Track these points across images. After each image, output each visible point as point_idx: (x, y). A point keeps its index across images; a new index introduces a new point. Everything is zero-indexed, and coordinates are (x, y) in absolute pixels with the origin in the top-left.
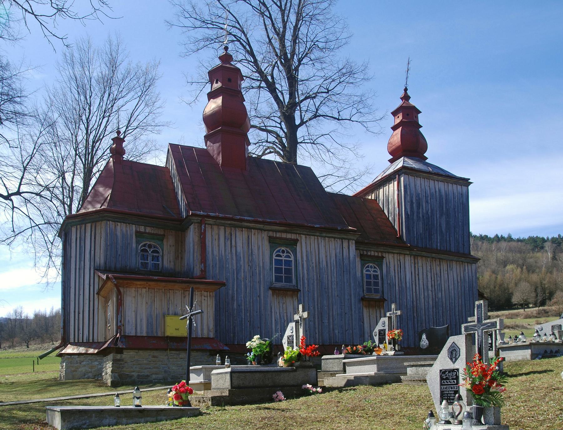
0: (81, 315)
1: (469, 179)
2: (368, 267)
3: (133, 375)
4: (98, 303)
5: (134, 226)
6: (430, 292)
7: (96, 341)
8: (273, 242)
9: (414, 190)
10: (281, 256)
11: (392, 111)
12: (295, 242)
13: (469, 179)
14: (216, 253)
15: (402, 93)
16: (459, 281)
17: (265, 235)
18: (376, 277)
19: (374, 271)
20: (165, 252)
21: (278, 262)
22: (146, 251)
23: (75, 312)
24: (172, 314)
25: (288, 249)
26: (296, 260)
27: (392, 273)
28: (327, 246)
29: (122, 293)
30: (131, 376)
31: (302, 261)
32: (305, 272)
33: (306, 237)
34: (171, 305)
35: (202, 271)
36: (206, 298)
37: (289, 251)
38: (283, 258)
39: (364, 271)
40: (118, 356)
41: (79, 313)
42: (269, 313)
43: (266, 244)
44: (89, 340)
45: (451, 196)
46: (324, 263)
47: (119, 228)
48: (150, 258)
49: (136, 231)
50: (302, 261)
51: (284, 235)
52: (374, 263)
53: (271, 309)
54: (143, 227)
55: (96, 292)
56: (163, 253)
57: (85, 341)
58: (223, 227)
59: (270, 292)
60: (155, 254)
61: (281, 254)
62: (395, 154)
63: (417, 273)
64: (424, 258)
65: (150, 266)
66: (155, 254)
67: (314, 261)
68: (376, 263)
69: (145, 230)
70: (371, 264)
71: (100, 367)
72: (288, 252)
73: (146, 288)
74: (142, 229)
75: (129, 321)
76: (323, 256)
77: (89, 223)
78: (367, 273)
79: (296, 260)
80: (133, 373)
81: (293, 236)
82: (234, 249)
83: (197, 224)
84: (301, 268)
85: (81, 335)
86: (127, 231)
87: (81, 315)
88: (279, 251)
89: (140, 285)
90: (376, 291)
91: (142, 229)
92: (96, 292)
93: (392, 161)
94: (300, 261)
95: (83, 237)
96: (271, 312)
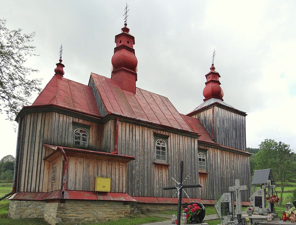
0: (30, 174)
1: (246, 113)
3: (72, 219)
4: (44, 167)
5: (72, 118)
6: (229, 170)
7: (40, 191)
8: (155, 135)
9: (56, 140)
11: (206, 75)
14: (124, 138)
15: (211, 66)
16: (242, 165)
17: (152, 131)
19: (203, 157)
20: (91, 137)
21: (158, 148)
22: (79, 134)
23: (26, 171)
24: (100, 176)
29: (67, 160)
30: (71, 220)
31: (171, 148)
36: (122, 167)
38: (161, 146)
40: (62, 205)
41: (29, 172)
42: (153, 177)
43: (152, 136)
44: (35, 190)
46: (182, 150)
47: (61, 119)
48: (81, 139)
49: (73, 121)
50: (171, 148)
51: (162, 132)
52: (203, 153)
54: (77, 119)
55: (43, 158)
57: (32, 191)
58: (129, 124)
59: (153, 166)
60: (84, 137)
61: (160, 143)
62: (207, 97)
64: (226, 152)
66: (84, 137)
68: (204, 152)
69: (79, 121)
70: (201, 153)
71: (43, 210)
73: (83, 158)
74: (77, 120)
75: (71, 180)
76: (181, 146)
77: (40, 112)
78: (203, 158)
80: (72, 217)
81: (167, 134)
83: (113, 120)
85: (29, 187)
87: (30, 174)
89: (80, 155)
91: (77, 120)
92: (43, 158)
93: (205, 100)
96: (154, 177)
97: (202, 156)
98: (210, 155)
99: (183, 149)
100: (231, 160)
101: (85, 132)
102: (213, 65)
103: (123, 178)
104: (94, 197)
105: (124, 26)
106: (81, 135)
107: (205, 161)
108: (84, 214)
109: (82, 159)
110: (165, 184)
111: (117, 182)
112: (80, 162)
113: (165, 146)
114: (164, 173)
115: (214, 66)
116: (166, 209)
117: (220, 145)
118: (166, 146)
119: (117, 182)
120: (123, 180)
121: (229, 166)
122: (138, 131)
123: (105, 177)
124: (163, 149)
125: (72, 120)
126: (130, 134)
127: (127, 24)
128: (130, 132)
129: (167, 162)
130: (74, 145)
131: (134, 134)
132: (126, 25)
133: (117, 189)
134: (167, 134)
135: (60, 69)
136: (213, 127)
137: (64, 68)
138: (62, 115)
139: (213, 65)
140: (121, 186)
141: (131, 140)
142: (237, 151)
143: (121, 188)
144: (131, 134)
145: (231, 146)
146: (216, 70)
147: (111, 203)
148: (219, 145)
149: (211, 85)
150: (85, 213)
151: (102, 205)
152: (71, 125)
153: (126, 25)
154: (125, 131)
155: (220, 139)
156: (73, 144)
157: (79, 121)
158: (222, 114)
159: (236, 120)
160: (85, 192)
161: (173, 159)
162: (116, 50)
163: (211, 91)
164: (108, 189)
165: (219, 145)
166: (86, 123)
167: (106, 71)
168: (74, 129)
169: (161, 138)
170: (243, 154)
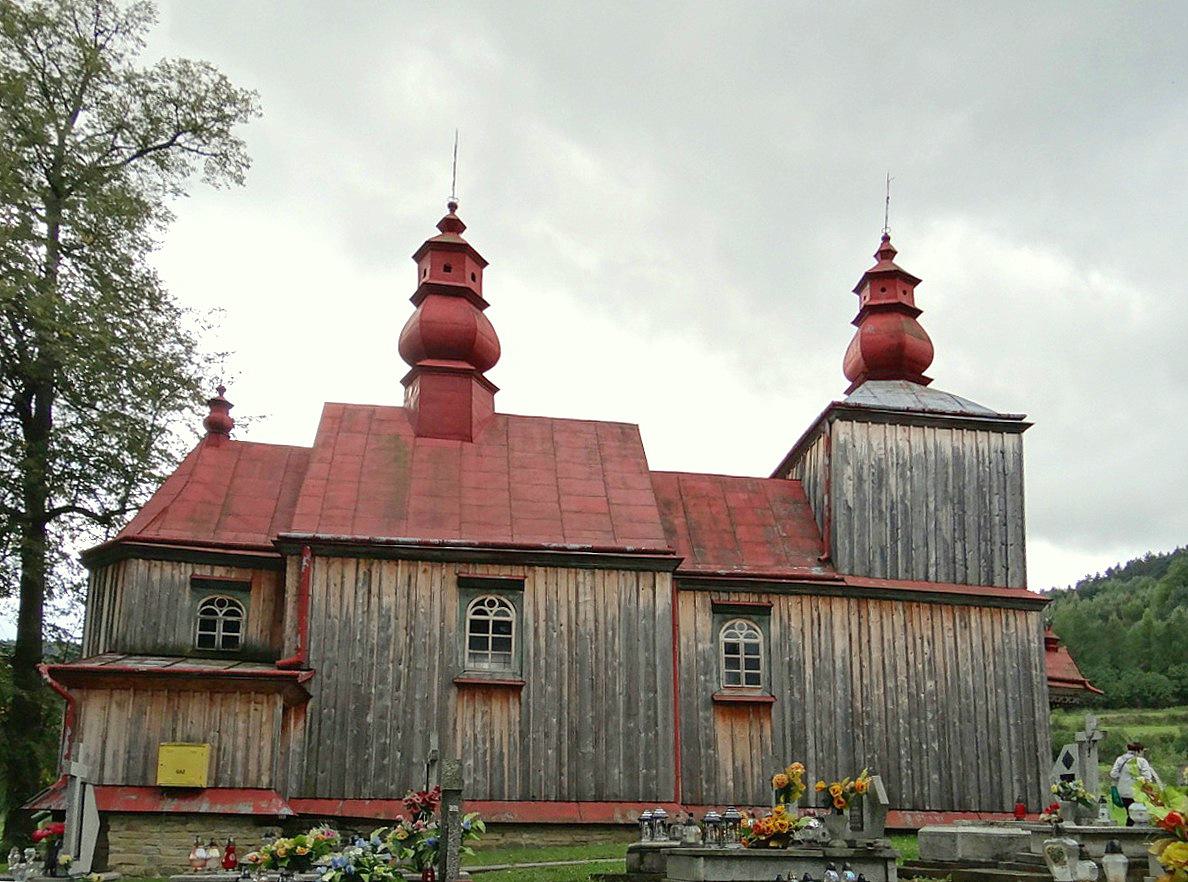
1: (1024, 417)
2: (732, 627)
8: (465, 584)
10: (485, 613)
12: (766, 610)
13: (1024, 417)
18: (752, 649)
25: (502, 598)
26: (521, 621)
27: (795, 637)
28: (599, 588)
31: (536, 621)
32: (542, 643)
33: (546, 571)
34: (180, 722)
35: (297, 649)
37: (506, 601)
39: (722, 636)
43: (452, 590)
45: (969, 459)
46: (591, 625)
47: (156, 576)
48: (220, 626)
50: (536, 621)
52: (750, 619)
53: (455, 724)
54: (208, 568)
56: (248, 617)
59: (454, 692)
60: (229, 619)
61: (487, 609)
63: (865, 640)
64: (886, 604)
65: (219, 641)
66: (229, 619)
67: (564, 620)
69: (212, 572)
72: (502, 604)
76: (587, 610)
79: (521, 621)
82: (374, 600)
84: (532, 634)
86: (173, 576)
88: (481, 603)
90: (753, 679)
94: (531, 622)
95: (101, 591)
96: (455, 729)
97: (745, 632)
98: (786, 629)
99: (596, 621)
100: (918, 636)
101: (232, 603)
102: (886, 238)
103: (260, 741)
104: (147, 804)
105: (447, 212)
106: (221, 615)
107: (762, 652)
108: (118, 852)
109: (125, 695)
110: (502, 753)
111: (240, 755)
112: (120, 705)
113: (508, 616)
114: (503, 717)
115: (891, 242)
116: (501, 842)
117: (843, 580)
118: (512, 617)
119: (240, 755)
120: (260, 749)
121: (901, 665)
122: (390, 579)
123: (199, 741)
124: (503, 627)
125: (190, 573)
126: (360, 594)
127: (458, 204)
128: (360, 584)
129: (519, 673)
130: (197, 647)
131: (375, 590)
132: (453, 207)
133: (239, 779)
134: (517, 572)
135: (217, 415)
136: (828, 506)
137: (230, 411)
138: (158, 563)
139: (886, 238)
140: (253, 767)
141: (364, 612)
142: (949, 596)
143: (253, 776)
144: (364, 593)
145: (921, 576)
146: (901, 262)
147: (210, 821)
148: (837, 580)
149: (877, 324)
150: (122, 850)
151: (176, 828)
152: (188, 588)
153: (453, 207)
154: (339, 586)
155: (859, 552)
156: (194, 646)
157: (212, 572)
158: (875, 444)
159: (958, 458)
160: (132, 789)
161: (542, 662)
162: (417, 299)
163: (860, 354)
164: (200, 780)
165: (837, 580)
166: (234, 575)
167: (384, 382)
168: (195, 599)
169: (494, 591)
170: (995, 604)
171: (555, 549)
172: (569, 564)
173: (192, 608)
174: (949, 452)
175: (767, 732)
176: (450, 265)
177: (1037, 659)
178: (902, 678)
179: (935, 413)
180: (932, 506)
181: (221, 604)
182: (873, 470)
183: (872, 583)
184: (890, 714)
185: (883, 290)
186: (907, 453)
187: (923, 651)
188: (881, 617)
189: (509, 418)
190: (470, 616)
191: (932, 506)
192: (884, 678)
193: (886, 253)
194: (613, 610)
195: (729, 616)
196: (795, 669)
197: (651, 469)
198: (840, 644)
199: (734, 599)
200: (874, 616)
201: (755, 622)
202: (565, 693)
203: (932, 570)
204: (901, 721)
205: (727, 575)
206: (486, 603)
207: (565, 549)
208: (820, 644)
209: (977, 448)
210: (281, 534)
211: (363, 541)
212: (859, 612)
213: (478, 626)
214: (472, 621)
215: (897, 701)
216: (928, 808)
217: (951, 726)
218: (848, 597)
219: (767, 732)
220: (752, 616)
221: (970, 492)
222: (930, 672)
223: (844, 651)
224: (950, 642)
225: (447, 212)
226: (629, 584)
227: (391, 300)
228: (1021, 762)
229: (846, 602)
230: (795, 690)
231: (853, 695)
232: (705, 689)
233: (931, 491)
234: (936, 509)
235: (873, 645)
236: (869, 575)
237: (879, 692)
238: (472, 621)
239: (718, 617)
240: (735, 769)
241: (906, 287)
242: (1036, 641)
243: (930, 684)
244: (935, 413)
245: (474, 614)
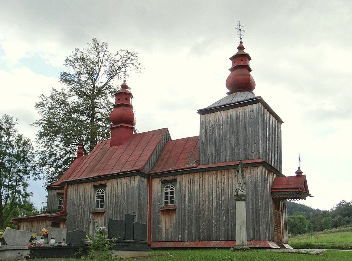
1: (197, 112)
10: (99, 194)
31: (109, 194)
37: (173, 186)
50: (109, 194)
52: (172, 184)
64: (210, 172)
72: (172, 186)
97: (170, 188)
102: (241, 43)
118: (104, 194)
122: (81, 187)
139: (241, 43)
146: (246, 51)
168: (58, 198)
171: (112, 174)
172: (115, 177)
173: (58, 200)
174: (234, 117)
175: (174, 218)
176: (241, 61)
177: (260, 184)
178: (214, 196)
179: (229, 104)
180: (228, 136)
181: (169, 187)
182: (211, 129)
183: (209, 166)
184: (210, 209)
185: (242, 61)
186: (221, 120)
187: (221, 186)
188: (209, 177)
189: (144, 134)
190: (164, 191)
191: (228, 136)
192: (209, 198)
193: (241, 48)
194: (125, 189)
195: (166, 184)
196: (182, 198)
197: (172, 140)
198: (196, 188)
199: (168, 178)
200: (207, 177)
201: (173, 185)
202: (114, 212)
203: (228, 158)
204: (213, 211)
205: (163, 172)
206: (103, 192)
207: (114, 174)
208: (190, 189)
209: (244, 112)
210: (61, 181)
211: (75, 180)
212: (202, 176)
213: (166, 194)
214: (165, 192)
215: (212, 204)
216: (221, 240)
217: (230, 211)
218: (199, 172)
219: (174, 218)
220: (172, 183)
221: (241, 128)
222: (223, 193)
223: (197, 190)
224: (230, 182)
225: (123, 82)
226: (129, 180)
227: (225, 69)
228: (253, 222)
229: (198, 174)
230: (183, 204)
231: (199, 204)
232: (159, 207)
233: (228, 131)
234: (230, 137)
235: (206, 186)
236: (208, 164)
237: (207, 202)
238: (165, 192)
239: (163, 185)
240: (166, 230)
241: (127, 97)
242: (260, 177)
243: (223, 198)
244: (229, 104)
245: (97, 194)
